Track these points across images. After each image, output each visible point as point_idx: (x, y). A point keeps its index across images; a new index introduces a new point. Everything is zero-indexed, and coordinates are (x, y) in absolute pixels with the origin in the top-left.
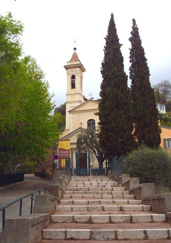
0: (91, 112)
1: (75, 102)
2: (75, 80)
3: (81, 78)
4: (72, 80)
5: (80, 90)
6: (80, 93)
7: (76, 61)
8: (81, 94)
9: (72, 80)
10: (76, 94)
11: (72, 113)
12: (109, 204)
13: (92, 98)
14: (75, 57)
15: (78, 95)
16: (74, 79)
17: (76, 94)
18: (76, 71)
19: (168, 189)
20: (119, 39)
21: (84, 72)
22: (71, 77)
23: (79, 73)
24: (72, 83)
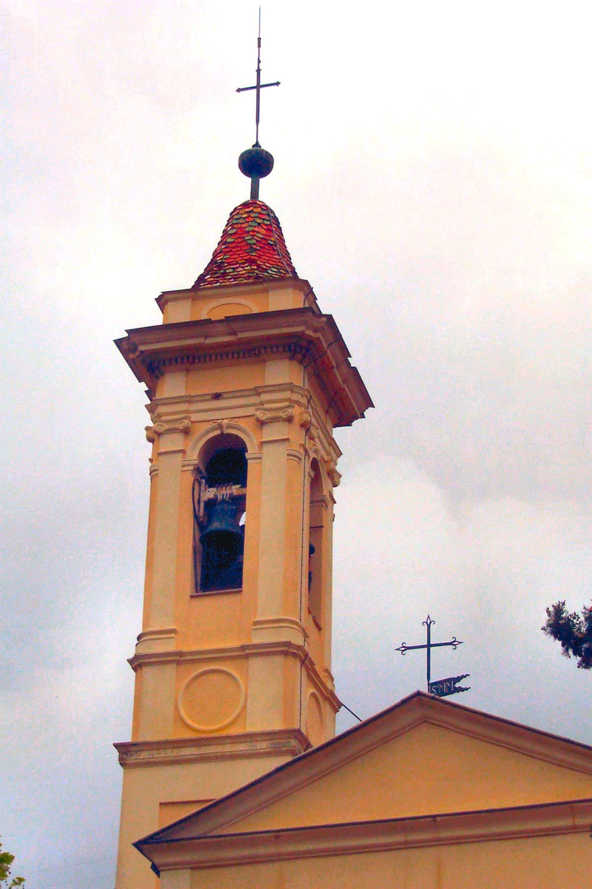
0: (430, 854)
1: (228, 748)
2: (239, 504)
3: (315, 482)
4: (210, 493)
5: (299, 613)
6: (298, 640)
7: (258, 280)
8: (306, 661)
9: (210, 493)
10: (246, 653)
11: (195, 867)
12: (265, 285)
13: (450, 685)
14: (257, 142)
15: (278, 660)
16: (235, 490)
17: (246, 653)
18: (257, 391)
19: (579, 629)
20: (162, 292)
21: (346, 418)
22: (194, 456)
23: (296, 411)
24: (201, 524)
